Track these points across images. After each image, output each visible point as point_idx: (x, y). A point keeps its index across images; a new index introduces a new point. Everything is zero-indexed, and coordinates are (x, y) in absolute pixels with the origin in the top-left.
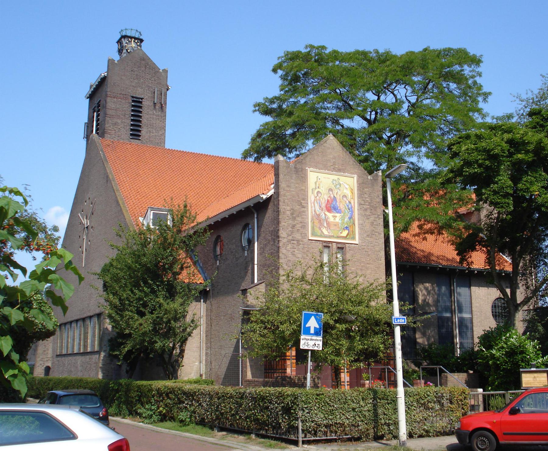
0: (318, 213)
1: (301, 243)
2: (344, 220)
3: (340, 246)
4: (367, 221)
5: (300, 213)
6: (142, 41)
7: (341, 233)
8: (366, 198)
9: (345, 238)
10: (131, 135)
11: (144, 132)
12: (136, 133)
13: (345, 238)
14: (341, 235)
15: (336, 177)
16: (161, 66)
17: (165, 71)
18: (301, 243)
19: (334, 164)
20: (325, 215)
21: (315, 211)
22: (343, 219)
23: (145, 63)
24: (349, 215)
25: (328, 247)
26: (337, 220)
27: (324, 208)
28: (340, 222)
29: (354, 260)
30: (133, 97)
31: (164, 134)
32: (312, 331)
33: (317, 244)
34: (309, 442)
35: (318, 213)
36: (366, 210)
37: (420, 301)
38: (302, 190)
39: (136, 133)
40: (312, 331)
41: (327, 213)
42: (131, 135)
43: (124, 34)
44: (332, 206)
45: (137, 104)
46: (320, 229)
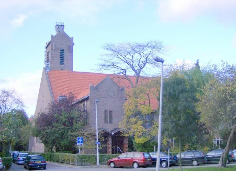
6: (64, 26)
10: (61, 63)
11: (65, 62)
12: (62, 62)
16: (71, 36)
17: (72, 38)
23: (65, 35)
30: (61, 49)
31: (72, 62)
32: (80, 142)
34: (72, 164)
37: (171, 140)
39: (62, 62)
40: (80, 142)
42: (61, 63)
43: (57, 24)
45: (62, 52)
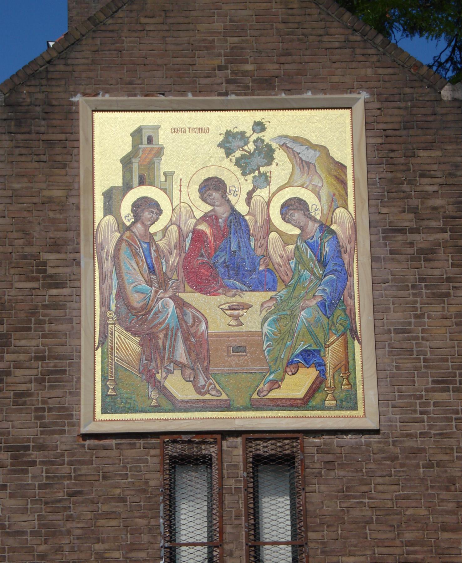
0: (136, 300)
1: (35, 455)
2: (293, 316)
3: (264, 448)
4: (436, 309)
5: (34, 312)
7: (275, 384)
8: (426, 196)
9: (303, 403)
13: (303, 403)
14: (274, 394)
15: (242, 120)
18: (35, 455)
19: (235, 56)
20: (181, 305)
21: (121, 294)
22: (282, 314)
24: (323, 291)
25: (205, 462)
26: (252, 322)
27: (178, 276)
28: (266, 329)
29: (356, 513)
33: (130, 453)
35: (136, 300)
36: (427, 254)
38: (50, 201)
41: (193, 298)
44: (222, 257)
46: (150, 377)
